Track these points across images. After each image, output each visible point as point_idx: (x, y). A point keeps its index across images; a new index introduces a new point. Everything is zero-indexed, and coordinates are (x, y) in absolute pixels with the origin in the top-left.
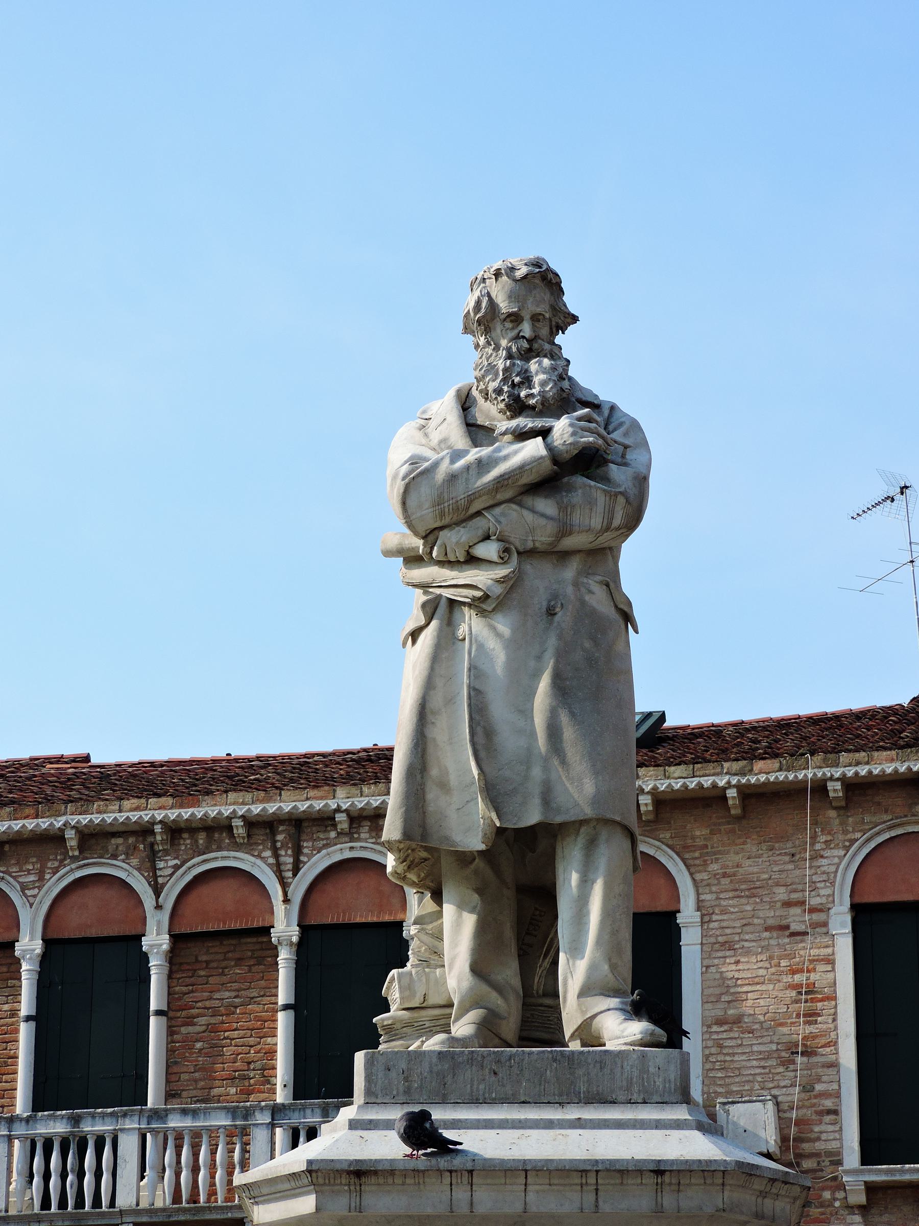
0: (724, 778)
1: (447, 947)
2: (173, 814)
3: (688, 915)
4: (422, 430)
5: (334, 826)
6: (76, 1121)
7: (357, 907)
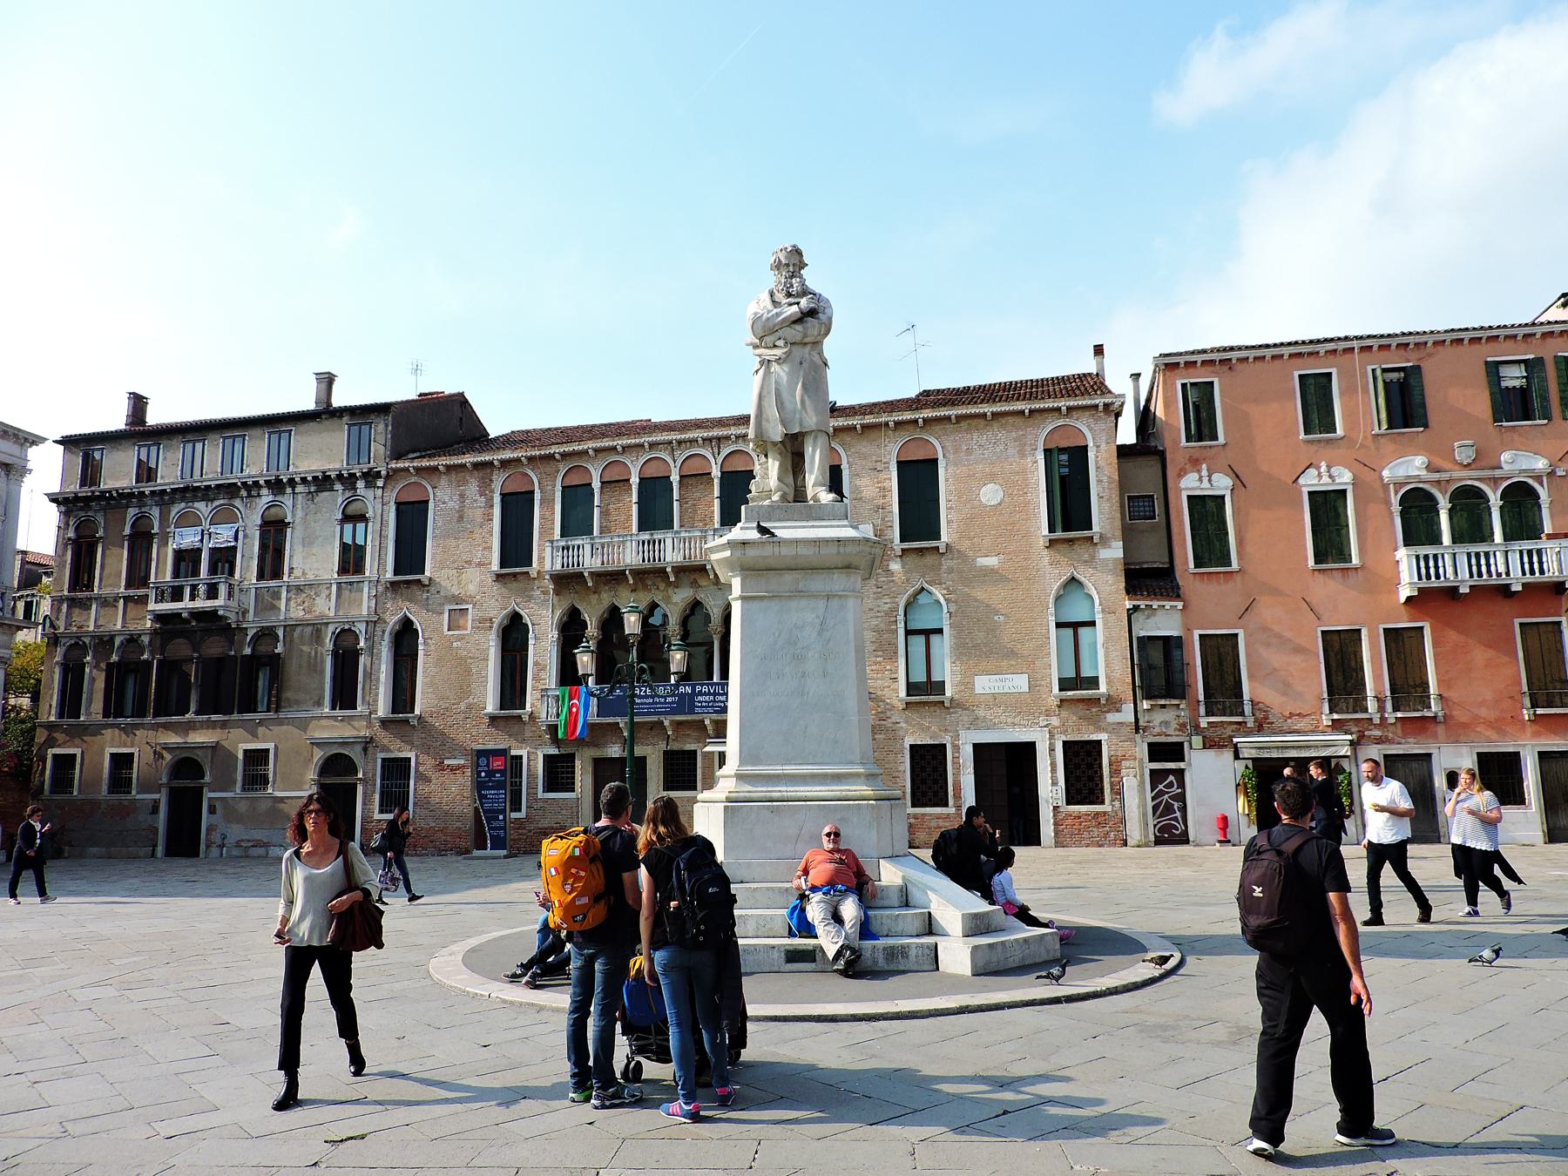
0: (855, 421)
1: (769, 474)
3: (844, 466)
4: (759, 304)
7: (738, 465)
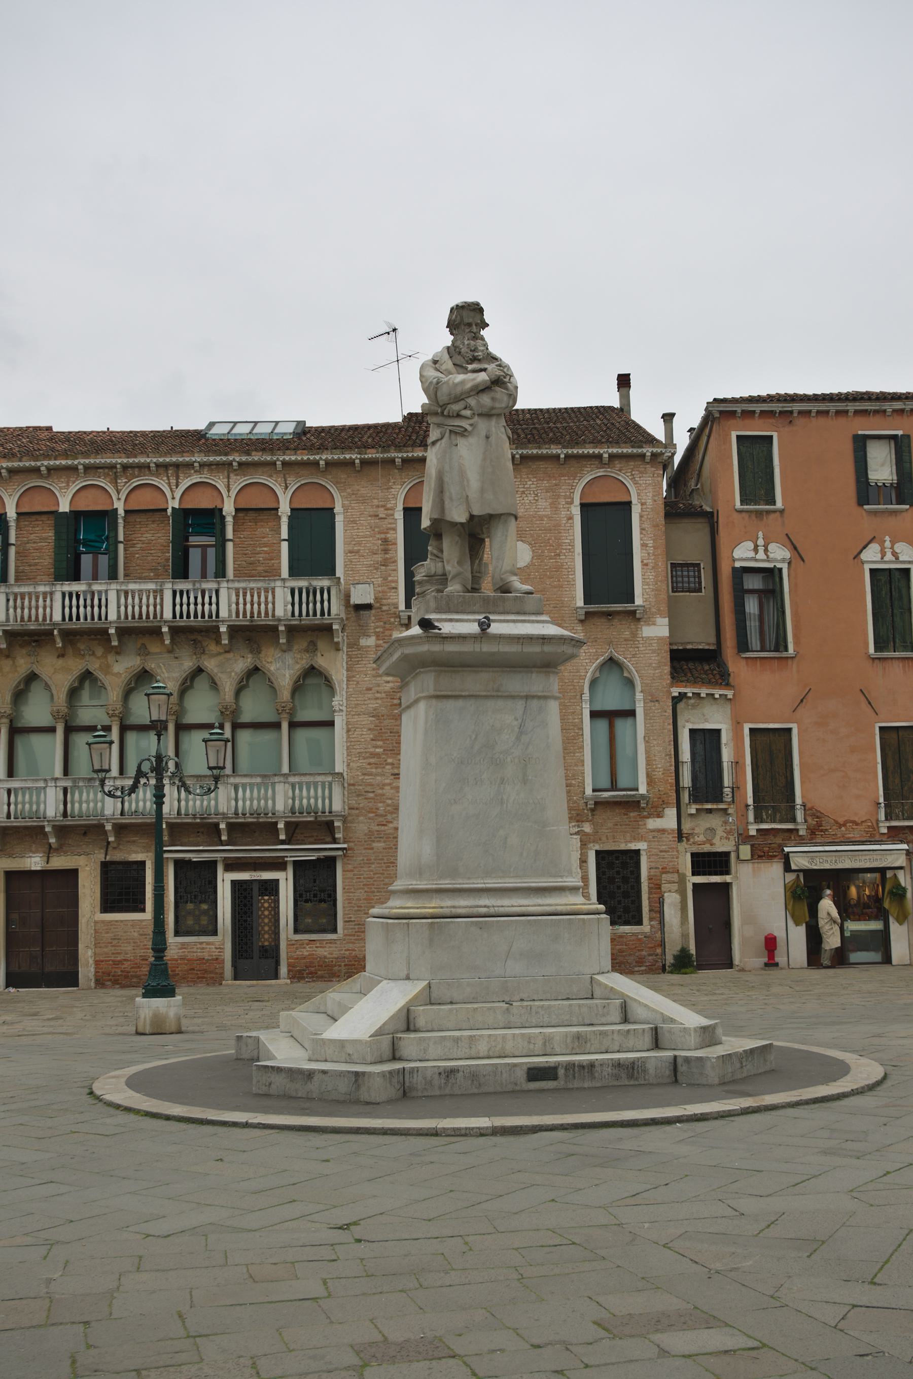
2: (125, 461)
3: (338, 509)
5: (194, 468)
6: (90, 585)
